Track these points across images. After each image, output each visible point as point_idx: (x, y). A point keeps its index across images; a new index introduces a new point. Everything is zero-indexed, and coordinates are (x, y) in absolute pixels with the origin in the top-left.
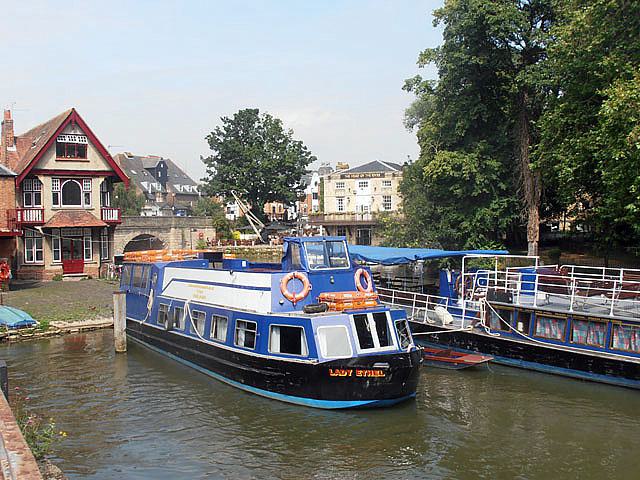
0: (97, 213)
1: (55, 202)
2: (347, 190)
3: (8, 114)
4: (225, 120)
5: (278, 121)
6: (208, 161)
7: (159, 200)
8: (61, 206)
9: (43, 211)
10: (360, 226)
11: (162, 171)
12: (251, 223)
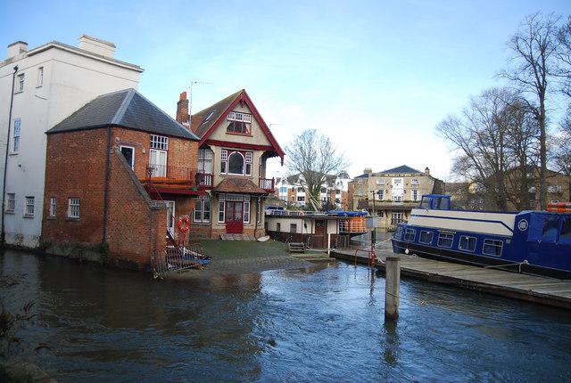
1: (223, 170)
3: (184, 95)
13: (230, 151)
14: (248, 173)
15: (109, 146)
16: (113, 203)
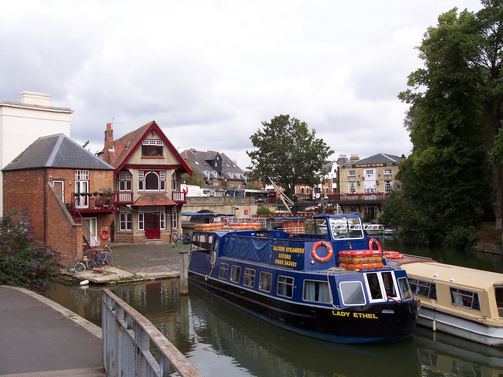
0: (169, 195)
1: (141, 187)
2: (357, 177)
3: (109, 126)
4: (266, 124)
5: (304, 124)
6: (252, 155)
7: (216, 184)
8: (144, 190)
9: (132, 194)
10: (369, 205)
11: (216, 162)
12: (284, 202)
13: (145, 172)
14: (162, 188)
15: (45, 182)
16: (50, 222)
